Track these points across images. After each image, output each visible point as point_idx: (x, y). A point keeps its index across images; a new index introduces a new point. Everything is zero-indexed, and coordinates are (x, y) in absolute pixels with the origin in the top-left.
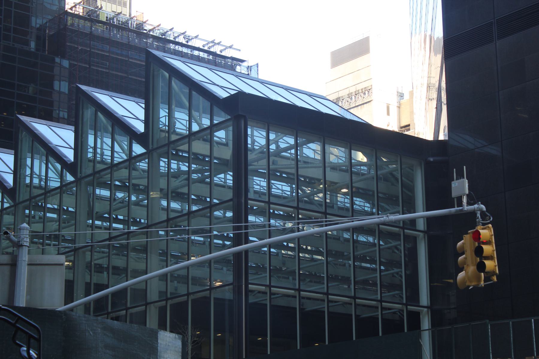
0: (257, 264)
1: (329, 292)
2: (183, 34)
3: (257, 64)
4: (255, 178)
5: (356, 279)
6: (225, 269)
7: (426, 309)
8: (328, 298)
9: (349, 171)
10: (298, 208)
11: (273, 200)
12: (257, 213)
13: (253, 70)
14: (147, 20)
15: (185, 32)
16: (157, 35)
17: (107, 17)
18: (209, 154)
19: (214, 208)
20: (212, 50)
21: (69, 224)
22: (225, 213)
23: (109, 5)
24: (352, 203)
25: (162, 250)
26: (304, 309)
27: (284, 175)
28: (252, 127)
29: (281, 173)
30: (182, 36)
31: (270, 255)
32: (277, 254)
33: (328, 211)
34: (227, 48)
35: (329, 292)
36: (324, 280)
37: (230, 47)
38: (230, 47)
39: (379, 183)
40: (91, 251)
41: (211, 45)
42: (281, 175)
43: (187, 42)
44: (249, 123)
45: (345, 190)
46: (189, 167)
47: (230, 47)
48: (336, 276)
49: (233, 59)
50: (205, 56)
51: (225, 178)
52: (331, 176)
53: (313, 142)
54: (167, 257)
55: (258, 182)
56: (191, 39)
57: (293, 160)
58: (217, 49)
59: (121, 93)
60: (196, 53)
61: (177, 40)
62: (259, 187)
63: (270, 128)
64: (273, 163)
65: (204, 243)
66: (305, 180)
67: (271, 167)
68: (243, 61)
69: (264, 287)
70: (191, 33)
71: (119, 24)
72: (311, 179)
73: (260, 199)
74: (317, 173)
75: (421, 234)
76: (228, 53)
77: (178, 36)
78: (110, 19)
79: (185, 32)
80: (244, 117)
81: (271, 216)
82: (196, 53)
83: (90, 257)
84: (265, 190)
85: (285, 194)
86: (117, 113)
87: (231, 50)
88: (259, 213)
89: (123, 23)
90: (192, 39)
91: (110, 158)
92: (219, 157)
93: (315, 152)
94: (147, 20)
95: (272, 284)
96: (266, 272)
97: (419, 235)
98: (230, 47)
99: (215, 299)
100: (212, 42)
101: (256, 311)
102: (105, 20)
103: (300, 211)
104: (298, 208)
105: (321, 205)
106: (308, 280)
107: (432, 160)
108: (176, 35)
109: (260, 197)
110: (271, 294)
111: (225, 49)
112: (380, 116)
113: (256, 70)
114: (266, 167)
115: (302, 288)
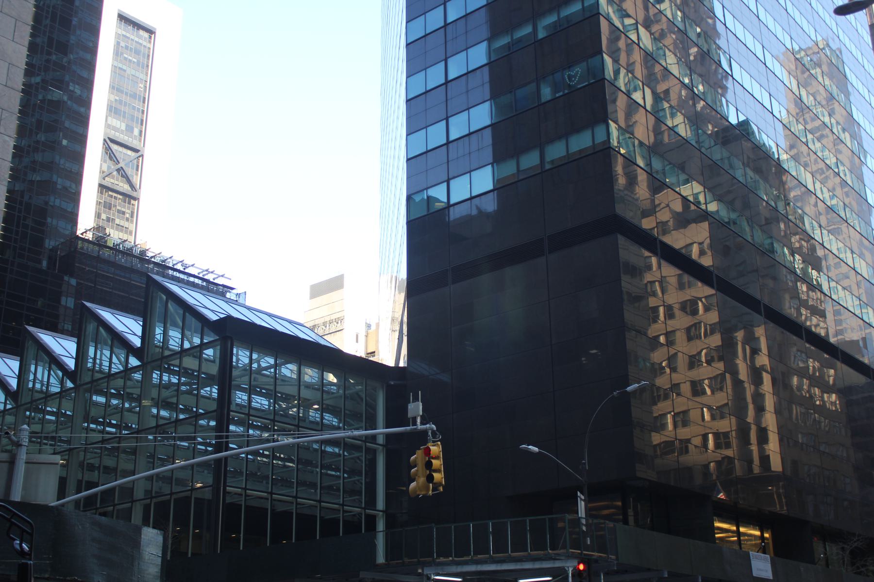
7: (381, 513)
11: (252, 412)
20: (206, 277)
22: (209, 422)
23: (117, 232)
32: (253, 460)
34: (209, 272)
42: (261, 391)
46: (179, 380)
52: (305, 393)
53: (290, 363)
58: (210, 277)
60: (192, 279)
64: (255, 380)
65: (188, 448)
68: (233, 289)
70: (188, 262)
72: (287, 395)
74: (292, 390)
75: (381, 448)
76: (219, 281)
81: (251, 426)
82: (192, 279)
89: (128, 249)
99: (196, 498)
110: (297, 504)
112: (350, 345)
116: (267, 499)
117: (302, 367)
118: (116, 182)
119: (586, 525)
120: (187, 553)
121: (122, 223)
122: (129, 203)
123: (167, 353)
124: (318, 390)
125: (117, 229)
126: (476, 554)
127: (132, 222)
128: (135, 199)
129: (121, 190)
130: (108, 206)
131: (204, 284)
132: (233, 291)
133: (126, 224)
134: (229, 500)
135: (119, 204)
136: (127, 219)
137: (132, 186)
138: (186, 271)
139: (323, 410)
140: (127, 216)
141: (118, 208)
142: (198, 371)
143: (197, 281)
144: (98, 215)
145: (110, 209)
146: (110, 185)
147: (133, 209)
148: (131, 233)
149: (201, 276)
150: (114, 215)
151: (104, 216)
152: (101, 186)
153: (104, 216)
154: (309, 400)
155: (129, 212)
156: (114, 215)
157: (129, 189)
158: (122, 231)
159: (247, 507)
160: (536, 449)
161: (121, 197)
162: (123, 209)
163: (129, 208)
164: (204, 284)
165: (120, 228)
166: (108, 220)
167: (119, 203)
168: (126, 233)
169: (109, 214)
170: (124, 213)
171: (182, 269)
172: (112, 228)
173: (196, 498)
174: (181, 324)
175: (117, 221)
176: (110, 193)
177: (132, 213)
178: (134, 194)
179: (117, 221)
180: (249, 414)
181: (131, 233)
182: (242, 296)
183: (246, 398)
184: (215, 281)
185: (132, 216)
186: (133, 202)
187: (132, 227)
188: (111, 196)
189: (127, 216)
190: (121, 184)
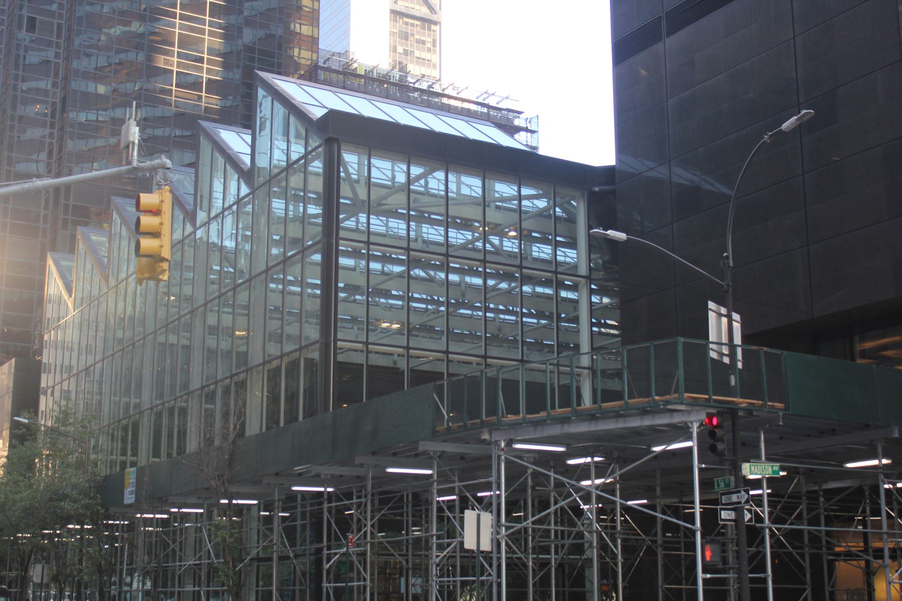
7: (586, 371)
8: (448, 357)
9: (406, 190)
11: (373, 239)
12: (347, 254)
18: (302, 187)
19: (307, 252)
20: (486, 102)
23: (417, 67)
24: (447, 237)
27: (534, 234)
28: (489, 179)
29: (430, 213)
32: (494, 319)
33: (371, 240)
34: (490, 95)
35: (450, 350)
39: (557, 225)
40: (233, 313)
41: (485, 96)
42: (429, 217)
45: (513, 234)
46: (473, 235)
49: (509, 110)
51: (358, 222)
52: (493, 216)
53: (438, 170)
57: (441, 197)
58: (492, 102)
59: (226, 124)
63: (372, 153)
64: (414, 201)
66: (461, 223)
68: (520, 113)
73: (427, 250)
74: (474, 213)
75: (583, 280)
80: (337, 140)
83: (123, 304)
86: (231, 149)
88: (354, 254)
89: (384, 76)
91: (405, 232)
95: (370, 341)
99: (503, 380)
100: (486, 93)
102: (363, 73)
104: (368, 243)
107: (597, 189)
112: (554, 144)
116: (403, 356)
117: (486, 180)
118: (412, 6)
119: (392, 323)
120: (18, 416)
122: (429, 29)
123: (276, 171)
124: (479, 204)
125: (418, 63)
126: (529, 412)
127: (435, 52)
128: (435, 23)
129: (418, 14)
130: (405, 36)
131: (485, 110)
132: (521, 116)
133: (428, 56)
134: (340, 358)
135: (418, 32)
136: (429, 50)
137: (431, 8)
138: (460, 96)
139: (524, 236)
140: (429, 45)
141: (417, 37)
142: (304, 191)
143: (473, 107)
144: (394, 49)
145: (407, 39)
146: (403, 10)
147: (435, 36)
148: (434, 66)
149: (480, 100)
150: (412, 46)
151: (400, 49)
152: (394, 12)
153: (400, 49)
154: (500, 225)
155: (430, 40)
156: (412, 46)
157: (428, 12)
158: (424, 65)
160: (622, 236)
161: (418, 23)
162: (423, 38)
163: (429, 36)
164: (485, 110)
165: (420, 61)
166: (406, 52)
167: (418, 32)
168: (429, 66)
169: (406, 45)
170: (424, 42)
172: (412, 62)
173: (503, 380)
174: (304, 133)
176: (406, 20)
177: (434, 41)
178: (434, 18)
179: (417, 53)
182: (534, 121)
184: (500, 106)
185: (434, 46)
186: (433, 27)
187: (435, 59)
188: (407, 24)
190: (417, 7)
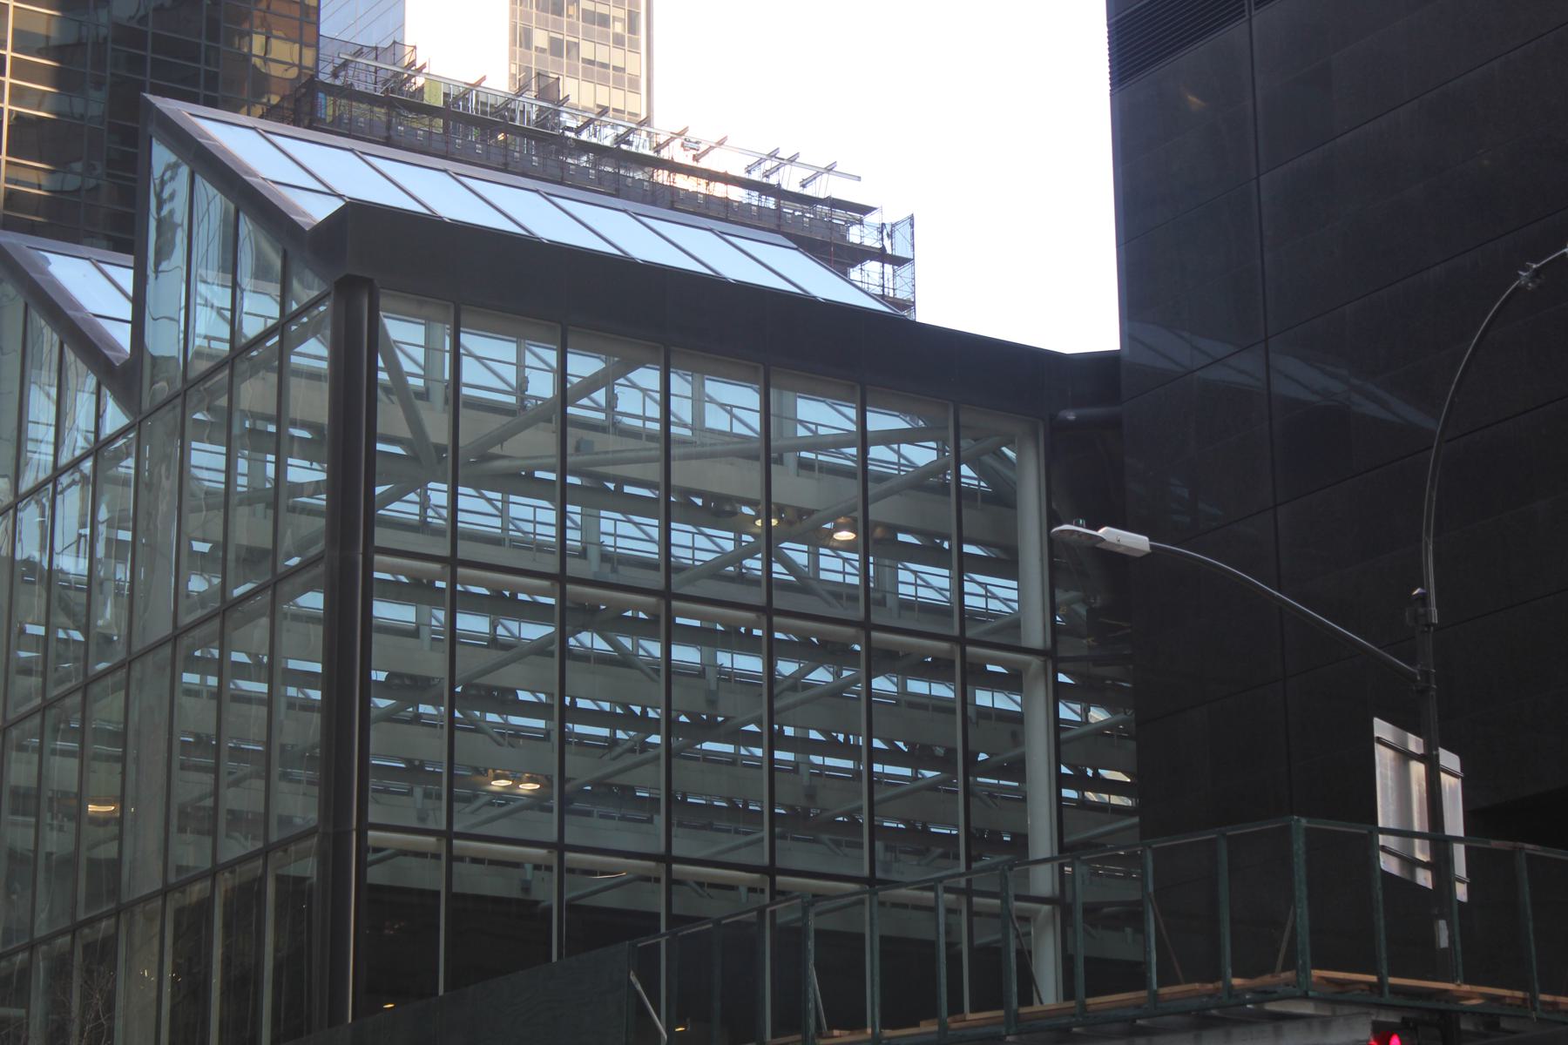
0: (409, 761)
1: (676, 852)
2: (680, 134)
3: (912, 218)
4: (603, 513)
5: (568, 787)
6: (418, 791)
7: (1046, 908)
9: (556, 418)
10: (667, 595)
11: (466, 550)
12: (396, 593)
13: (897, 235)
14: (484, 79)
15: (686, 130)
16: (607, 142)
17: (446, 95)
18: (272, 409)
19: (286, 588)
20: (773, 180)
21: (645, 756)
22: (1086, 711)
23: (587, 87)
24: (666, 543)
25: (729, 800)
26: (537, 903)
27: (902, 537)
29: (621, 481)
30: (678, 142)
31: (772, 770)
32: (795, 767)
34: (783, 162)
36: (958, 846)
37: (829, 170)
38: (829, 170)
41: (768, 165)
43: (696, 158)
44: (383, 302)
45: (845, 536)
46: (738, 541)
47: (829, 170)
48: (991, 832)
49: (834, 203)
50: (754, 198)
52: (790, 488)
53: (642, 364)
54: (217, 758)
55: (848, 569)
56: (706, 152)
57: (651, 437)
58: (790, 180)
60: (719, 190)
61: (665, 154)
62: (688, 553)
63: (464, 318)
64: (577, 449)
65: (547, 734)
67: (570, 459)
68: (866, 210)
69: (432, 839)
70: (703, 133)
71: (484, 113)
72: (721, 499)
73: (612, 578)
74: (741, 479)
75: (1035, 662)
76: (820, 189)
77: (667, 143)
78: (456, 99)
79: (686, 130)
80: (368, 283)
81: (457, 602)
82: (719, 190)
84: (440, 517)
85: (518, 530)
86: (78, 307)
87: (832, 178)
88: (416, 591)
89: (497, 110)
90: (711, 148)
92: (311, 419)
93: (733, 416)
94: (484, 79)
96: (762, 824)
97: (1029, 664)
98: (829, 170)
99: (818, 932)
100: (772, 156)
101: (397, 909)
102: (440, 103)
103: (776, 619)
104: (453, 562)
105: (855, 599)
106: (940, 850)
107: (1071, 416)
108: (662, 139)
109: (614, 570)
110: (972, 914)
111: (814, 178)
112: (954, 294)
113: (908, 237)
114: (555, 461)
115: (677, 851)
116: (549, 868)
119: (518, 780)
121: (602, 54)
123: (202, 366)
125: (588, 77)
127: (634, 47)
131: (771, 203)
132: (868, 219)
133: (617, 57)
136: (619, 41)
138: (704, 164)
139: (877, 544)
143: (737, 194)
144: (522, 38)
148: (634, 85)
149: (756, 176)
150: (572, 29)
151: (540, 39)
153: (540, 39)
154: (810, 512)
156: (572, 29)
158: (604, 81)
159: (453, 897)
160: (1138, 542)
162: (602, 9)
164: (771, 203)
165: (597, 71)
166: (556, 47)
168: (619, 85)
169: (558, 27)
170: (604, 21)
171: (689, 162)
172: (573, 74)
173: (818, 932)
175: (586, 50)
179: (586, 50)
180: (451, 566)
181: (634, 85)
183: (551, 516)
185: (633, 28)
187: (635, 64)
189: (618, 28)
